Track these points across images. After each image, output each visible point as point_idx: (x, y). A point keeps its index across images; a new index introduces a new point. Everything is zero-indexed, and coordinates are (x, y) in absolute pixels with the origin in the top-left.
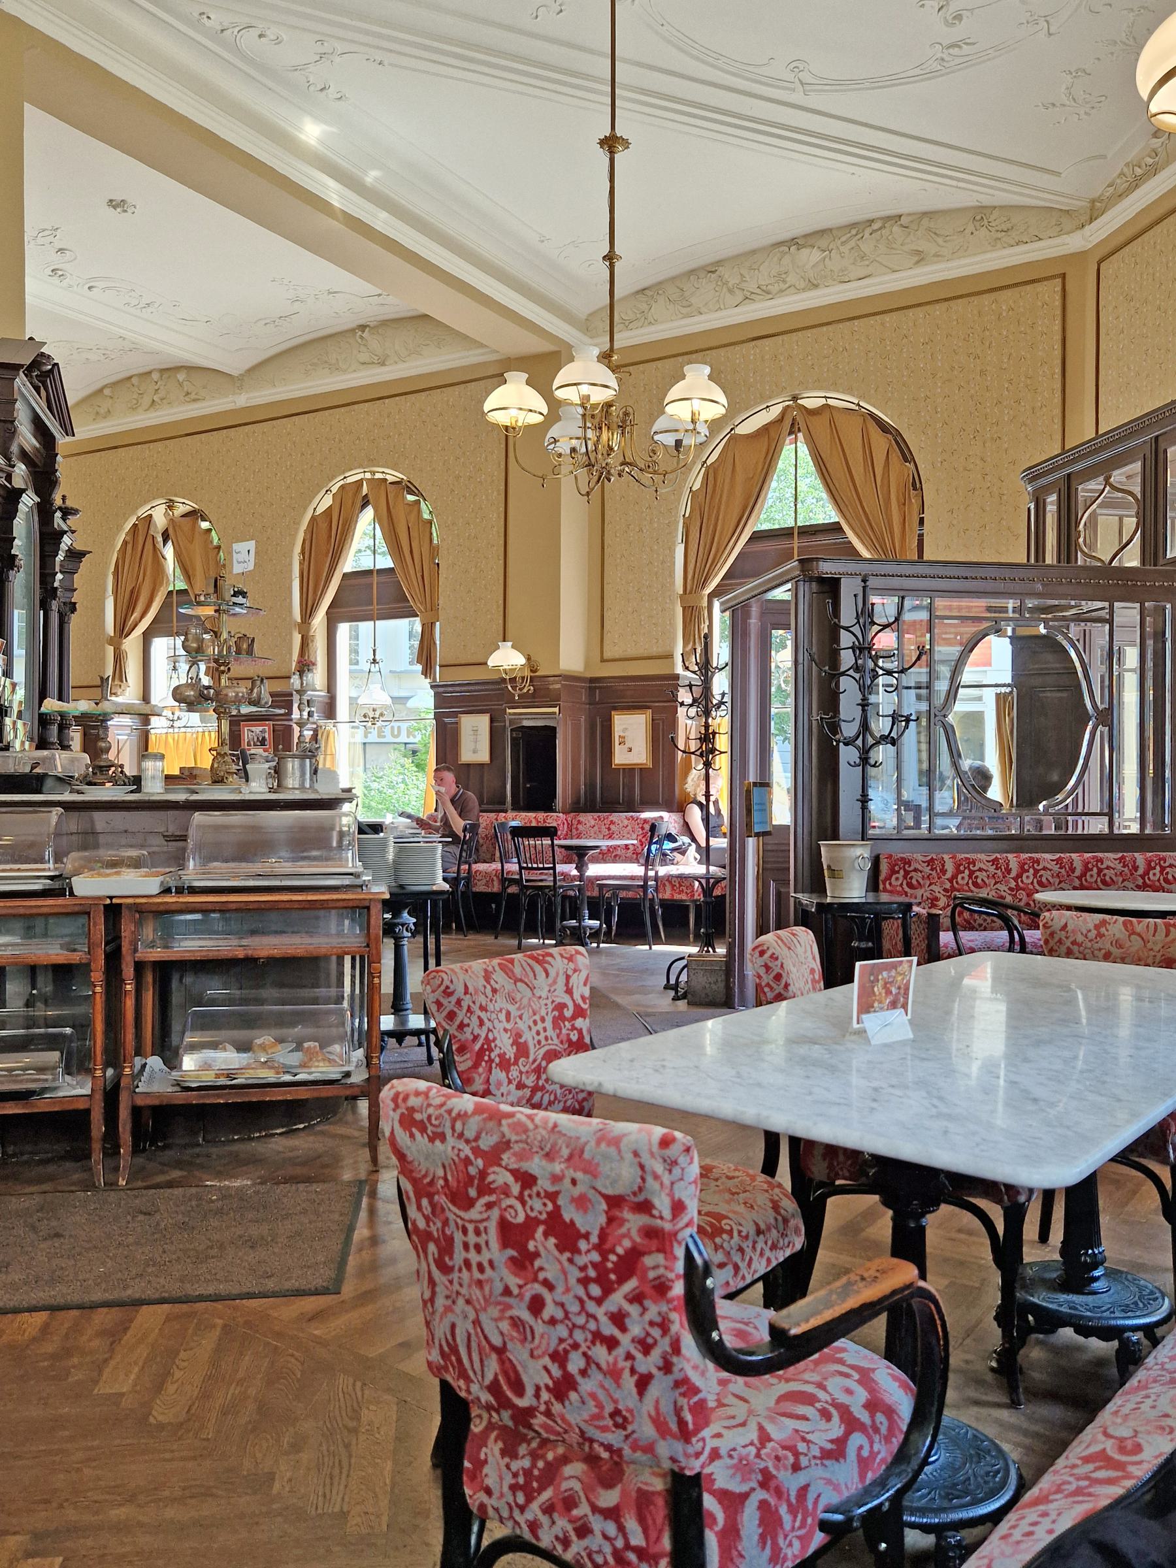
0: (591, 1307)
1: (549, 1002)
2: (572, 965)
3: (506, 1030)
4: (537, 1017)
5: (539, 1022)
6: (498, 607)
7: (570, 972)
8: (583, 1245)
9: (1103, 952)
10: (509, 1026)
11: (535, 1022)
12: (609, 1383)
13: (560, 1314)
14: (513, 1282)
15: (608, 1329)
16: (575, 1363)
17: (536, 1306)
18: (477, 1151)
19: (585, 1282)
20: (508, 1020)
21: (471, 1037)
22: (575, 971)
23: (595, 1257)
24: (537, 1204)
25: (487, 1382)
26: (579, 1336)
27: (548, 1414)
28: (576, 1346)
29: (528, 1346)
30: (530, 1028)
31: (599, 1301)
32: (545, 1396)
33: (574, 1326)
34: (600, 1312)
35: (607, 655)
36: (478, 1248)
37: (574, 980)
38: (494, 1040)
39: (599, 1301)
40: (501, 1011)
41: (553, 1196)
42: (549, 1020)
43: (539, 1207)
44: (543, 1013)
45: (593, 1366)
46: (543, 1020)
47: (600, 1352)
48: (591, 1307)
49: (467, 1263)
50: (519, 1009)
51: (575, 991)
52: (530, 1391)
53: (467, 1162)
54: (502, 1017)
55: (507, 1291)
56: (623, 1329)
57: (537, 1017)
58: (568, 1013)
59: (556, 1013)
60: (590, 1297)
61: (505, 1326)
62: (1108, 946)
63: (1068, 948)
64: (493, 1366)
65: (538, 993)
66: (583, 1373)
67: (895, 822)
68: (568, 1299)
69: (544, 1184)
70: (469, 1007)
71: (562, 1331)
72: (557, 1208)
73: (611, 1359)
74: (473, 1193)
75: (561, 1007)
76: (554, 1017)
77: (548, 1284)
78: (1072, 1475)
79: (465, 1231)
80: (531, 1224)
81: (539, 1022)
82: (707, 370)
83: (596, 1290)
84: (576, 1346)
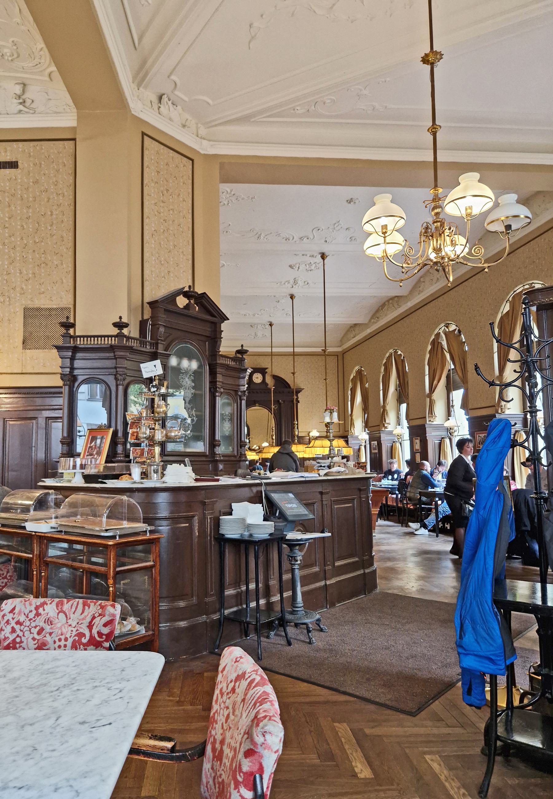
0: (21, 634)
1: (74, 630)
3: (34, 639)
4: (63, 637)
5: (63, 640)
6: (189, 193)
7: (96, 615)
10: (37, 637)
11: (60, 640)
15: (17, 627)
19: (21, 642)
20: (39, 633)
21: (3, 638)
22: (100, 615)
26: (28, 623)
29: (48, 616)
30: (55, 642)
33: (28, 627)
37: (97, 620)
38: (21, 642)
39: (18, 636)
40: (35, 627)
42: (70, 641)
44: (68, 636)
45: (26, 614)
46: (66, 640)
47: (22, 618)
50: (51, 628)
51: (94, 627)
54: (35, 631)
56: (13, 628)
57: (63, 637)
58: (84, 640)
59: (77, 638)
60: (20, 637)
65: (70, 622)
68: (27, 634)
70: (8, 620)
73: (20, 617)
75: (83, 635)
76: (74, 640)
81: (63, 640)
82: (390, 196)
83: (18, 640)
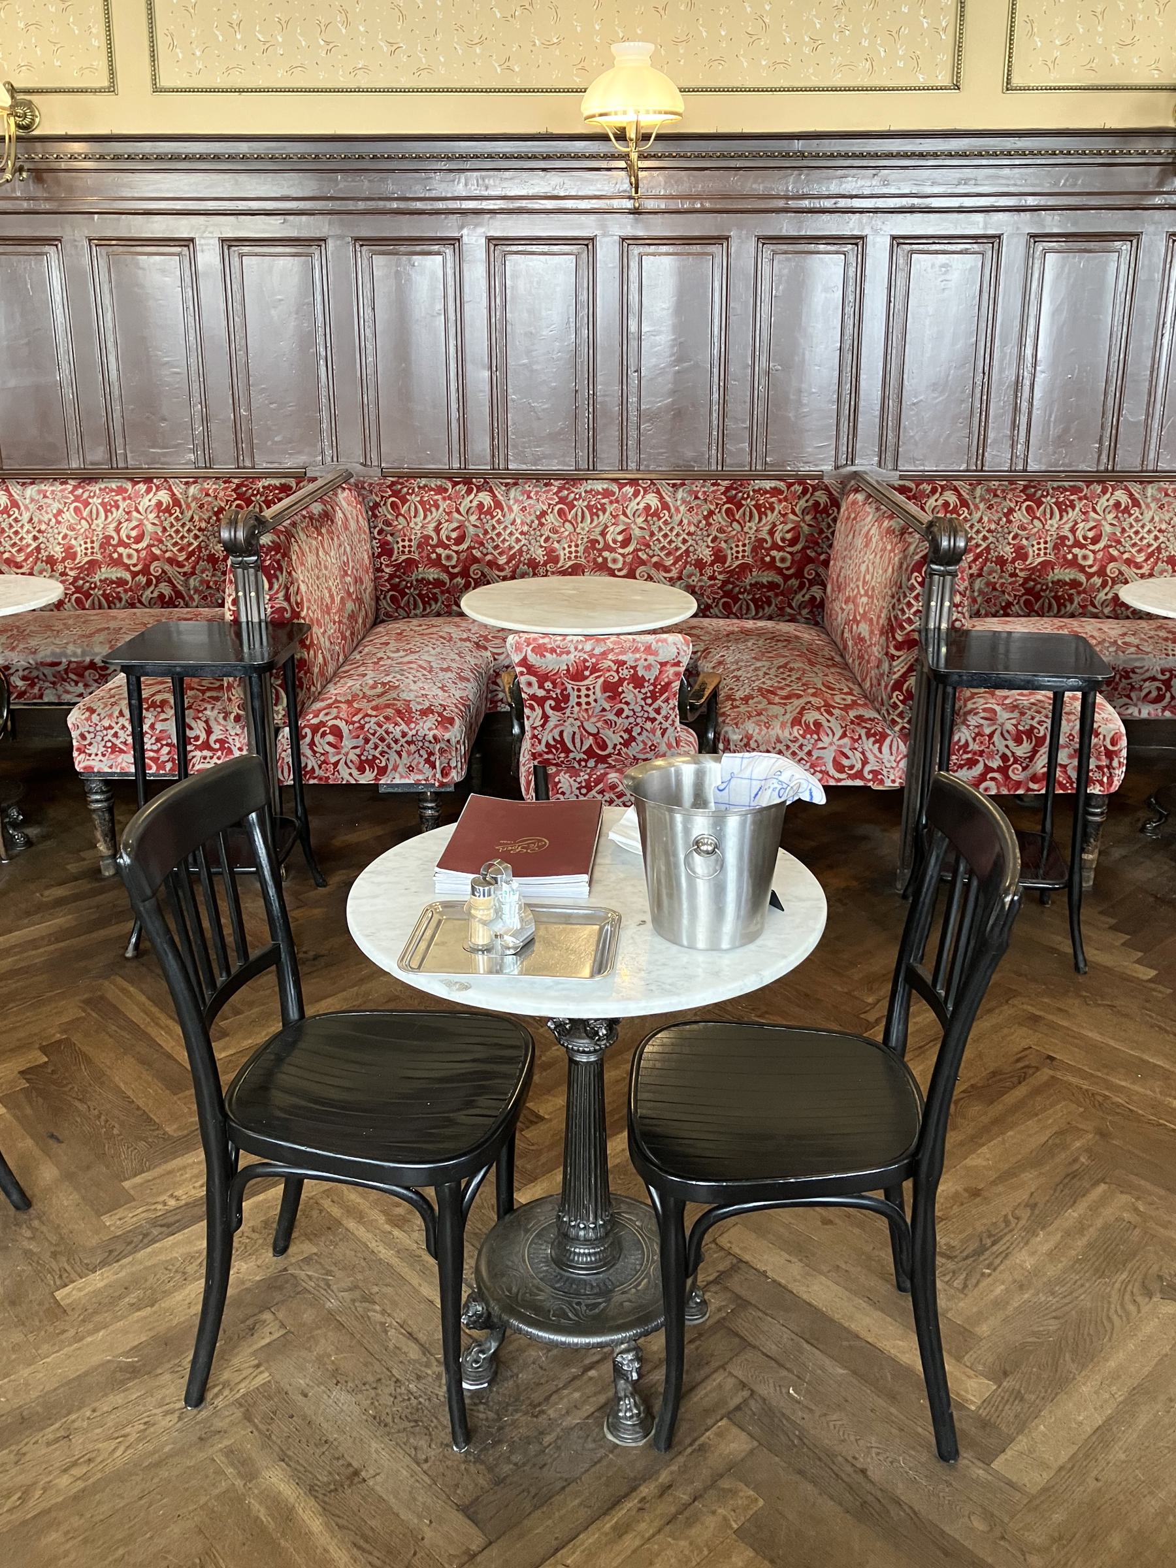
0: (646, 708)
2: (536, 732)
7: (540, 729)
8: (646, 684)
9: (624, 715)
12: (651, 735)
13: (631, 713)
14: (607, 706)
16: (637, 730)
17: (619, 713)
18: (591, 656)
23: (651, 688)
24: (626, 672)
25: (584, 749)
26: (639, 720)
27: (619, 754)
28: (637, 724)
31: (650, 705)
32: (618, 747)
34: (650, 709)
35: (944, 79)
36: (587, 696)
40: (627, 717)
41: (634, 668)
43: (625, 673)
48: (646, 708)
49: (579, 704)
52: (610, 746)
53: (585, 661)
55: (604, 710)
56: (659, 713)
61: (599, 724)
62: (619, 721)
63: (659, 713)
64: (591, 740)
66: (639, 734)
67: (678, 638)
69: (631, 663)
71: (631, 720)
72: (636, 672)
74: (587, 673)
77: (627, 703)
78: (879, 685)
79: (579, 690)
80: (621, 681)
83: (649, 701)
84: (637, 724)
